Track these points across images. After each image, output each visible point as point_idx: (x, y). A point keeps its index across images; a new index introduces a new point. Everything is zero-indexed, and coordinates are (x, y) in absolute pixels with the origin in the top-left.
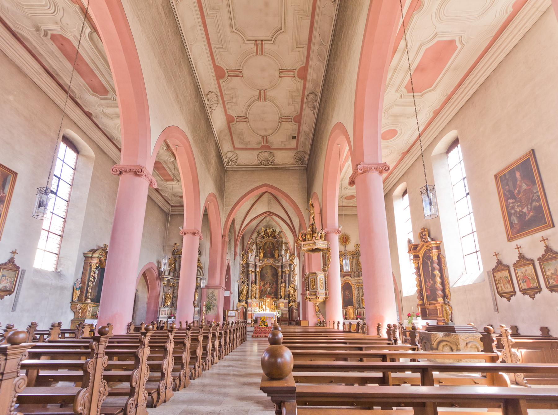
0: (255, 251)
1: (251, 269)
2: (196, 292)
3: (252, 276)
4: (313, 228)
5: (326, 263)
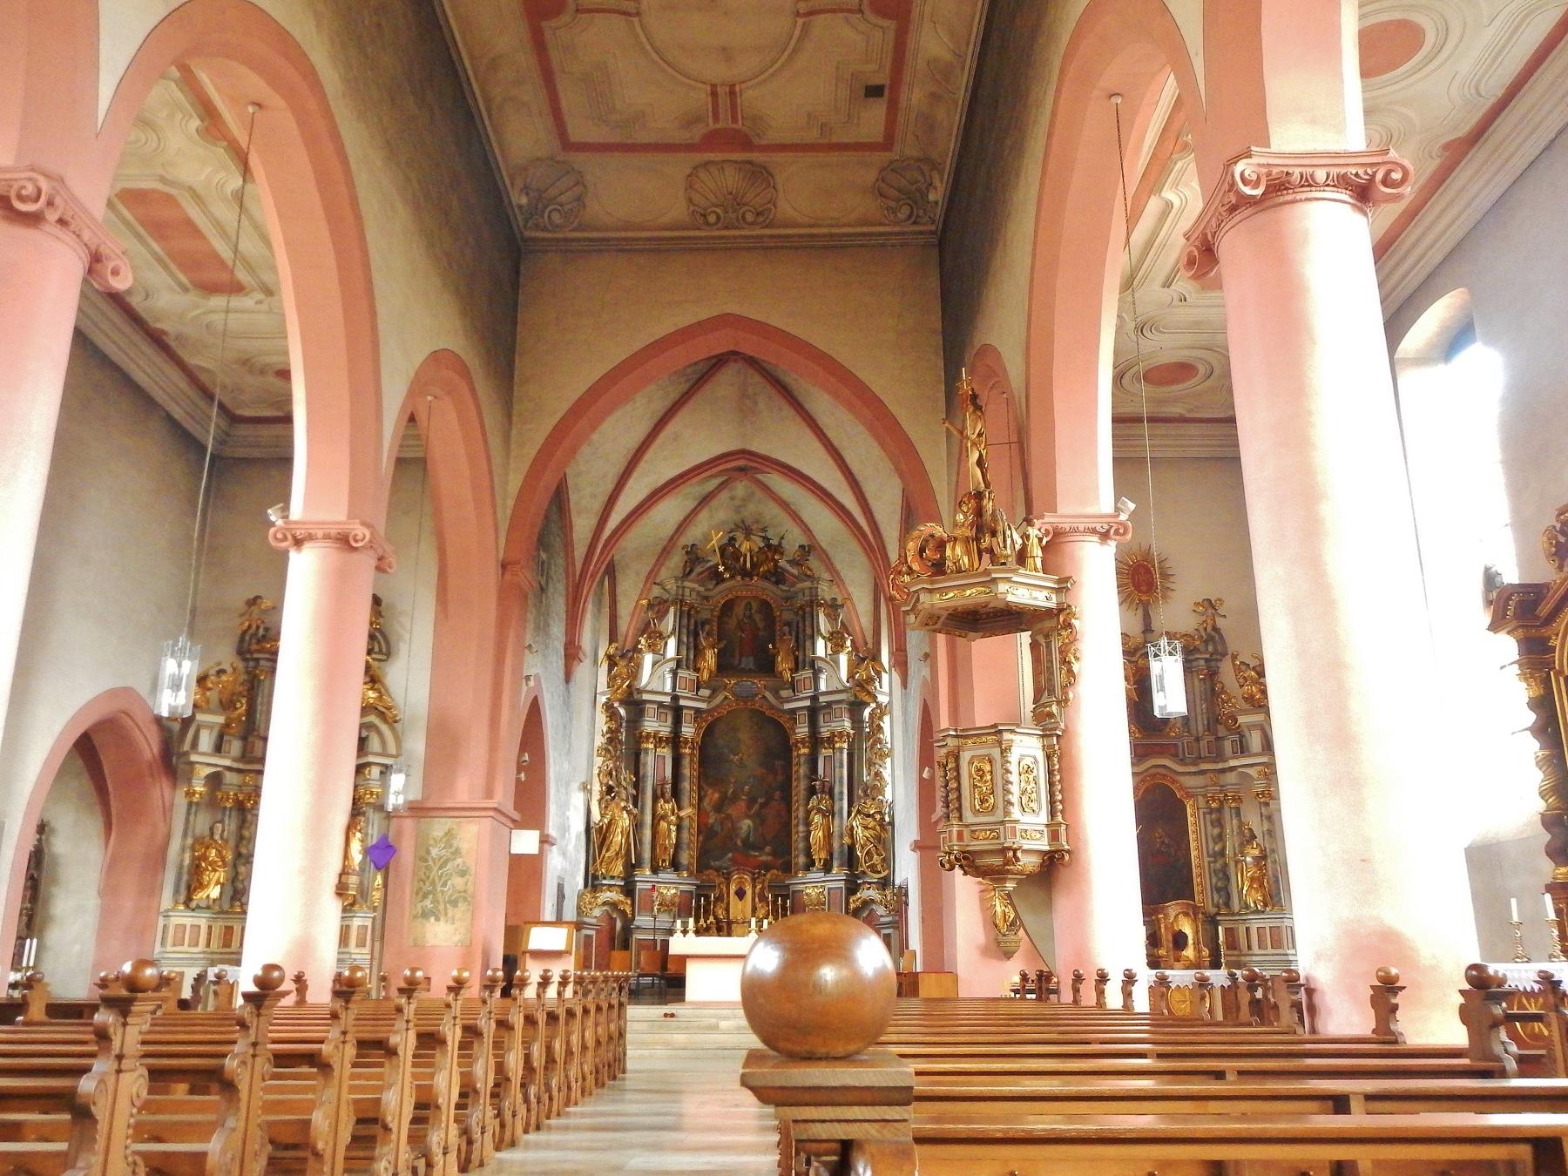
0: (672, 643)
1: (653, 724)
2: (350, 829)
3: (657, 763)
4: (979, 512)
5: (1054, 682)
